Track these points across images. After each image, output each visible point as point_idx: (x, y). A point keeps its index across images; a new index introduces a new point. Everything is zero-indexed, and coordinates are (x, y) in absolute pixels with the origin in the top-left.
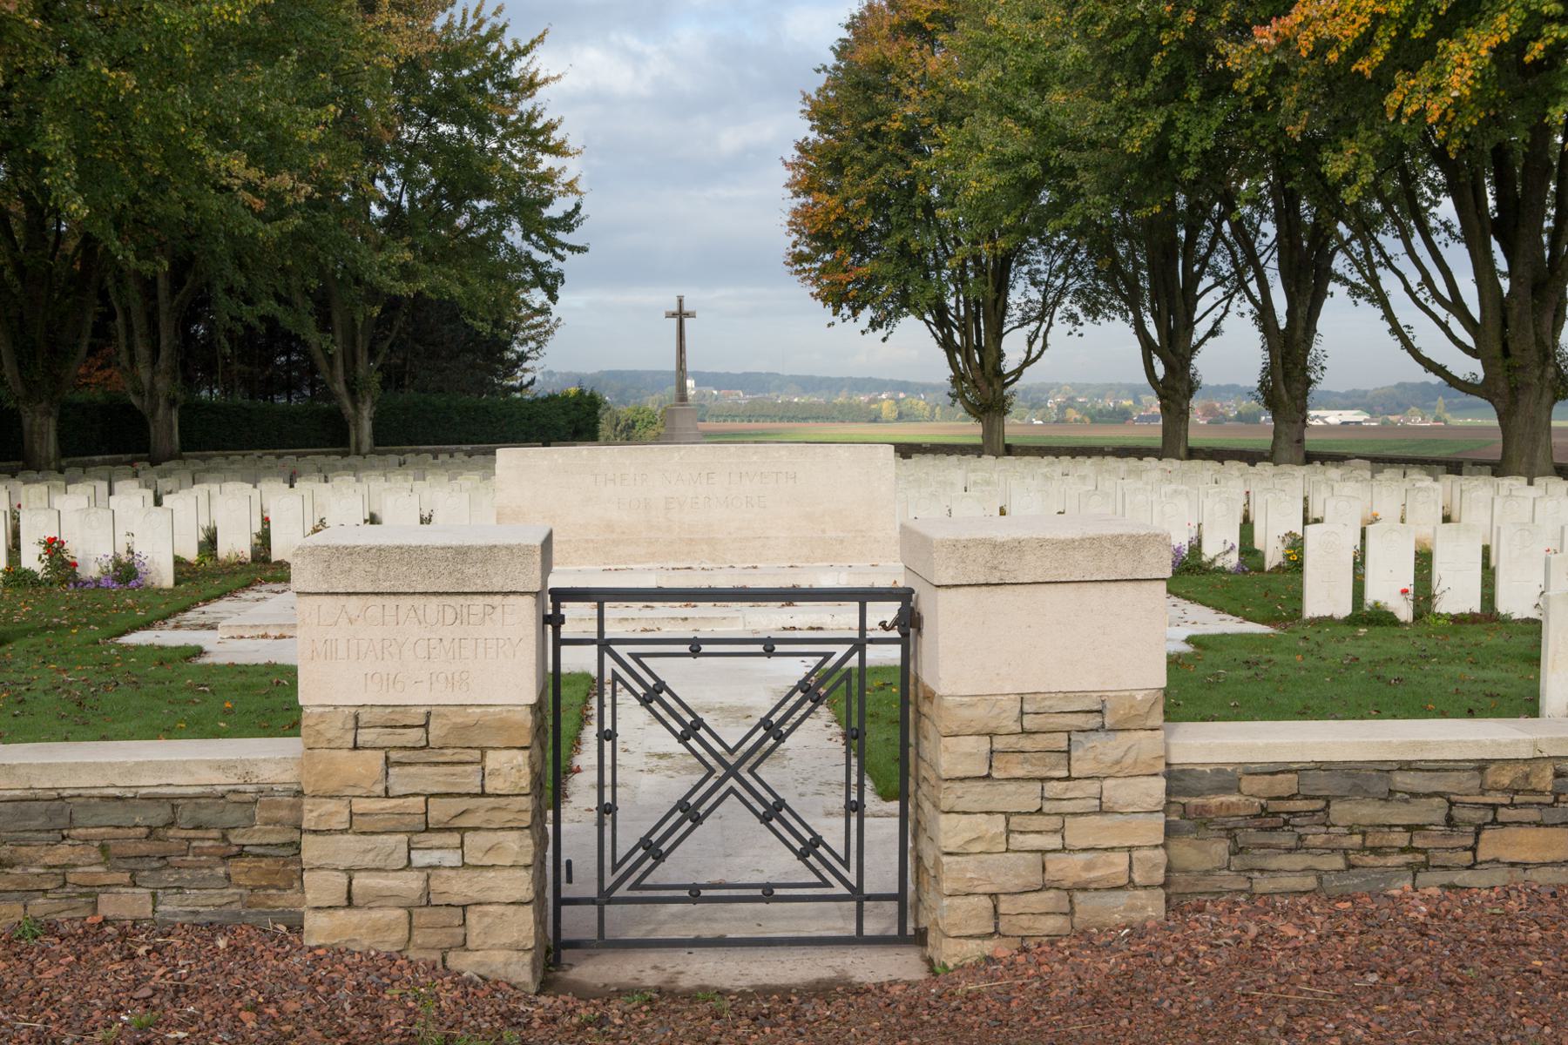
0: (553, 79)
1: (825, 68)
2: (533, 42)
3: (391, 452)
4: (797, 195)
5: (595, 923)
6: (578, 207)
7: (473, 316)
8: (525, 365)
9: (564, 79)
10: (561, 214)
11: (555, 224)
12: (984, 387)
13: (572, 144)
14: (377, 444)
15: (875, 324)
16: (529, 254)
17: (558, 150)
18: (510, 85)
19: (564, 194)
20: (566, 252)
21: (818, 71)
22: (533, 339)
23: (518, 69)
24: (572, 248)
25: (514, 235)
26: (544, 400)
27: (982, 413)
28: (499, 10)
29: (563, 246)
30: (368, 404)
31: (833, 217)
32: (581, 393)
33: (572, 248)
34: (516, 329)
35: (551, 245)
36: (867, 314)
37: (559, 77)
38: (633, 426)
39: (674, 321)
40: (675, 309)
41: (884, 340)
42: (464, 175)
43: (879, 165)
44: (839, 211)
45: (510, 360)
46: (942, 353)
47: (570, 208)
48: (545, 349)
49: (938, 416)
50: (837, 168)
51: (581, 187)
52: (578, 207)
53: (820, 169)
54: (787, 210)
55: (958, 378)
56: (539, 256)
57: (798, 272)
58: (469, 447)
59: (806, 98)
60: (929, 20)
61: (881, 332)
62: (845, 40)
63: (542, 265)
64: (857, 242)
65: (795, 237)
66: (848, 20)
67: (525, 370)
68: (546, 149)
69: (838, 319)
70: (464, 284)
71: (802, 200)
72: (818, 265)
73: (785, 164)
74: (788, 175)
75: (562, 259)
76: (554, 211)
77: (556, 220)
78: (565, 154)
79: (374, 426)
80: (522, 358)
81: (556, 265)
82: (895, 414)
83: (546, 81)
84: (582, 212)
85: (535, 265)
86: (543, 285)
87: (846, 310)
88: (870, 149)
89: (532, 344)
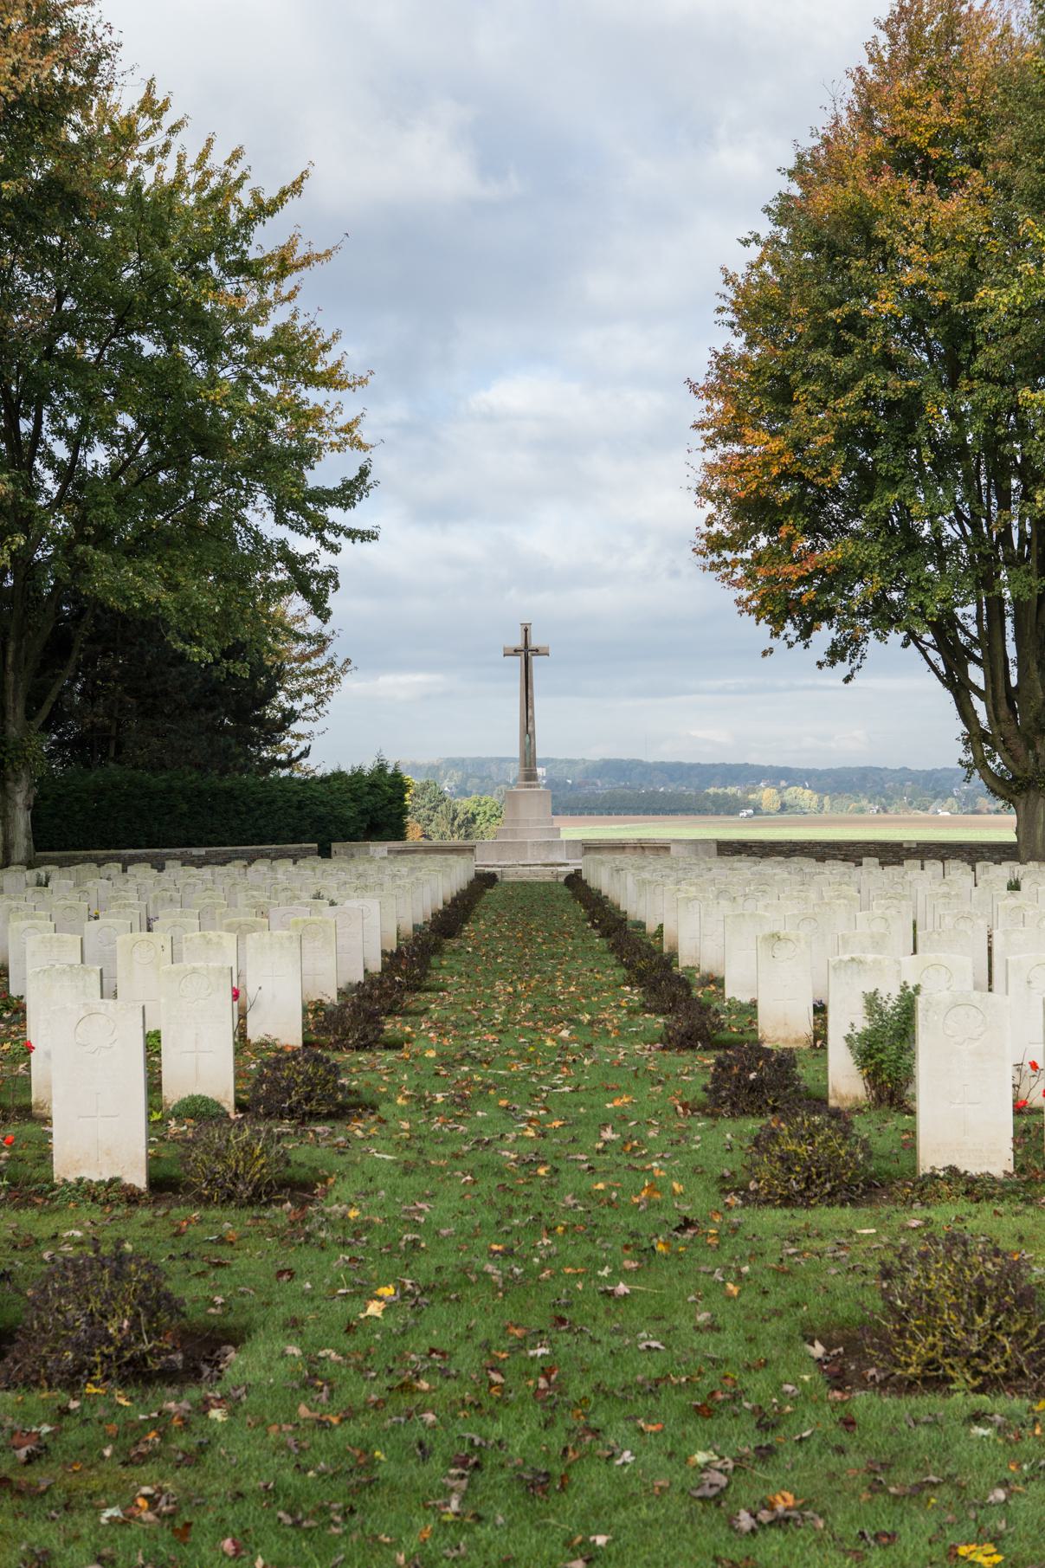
0: (319, 257)
1: (756, 239)
2: (284, 193)
3: (84, 860)
4: (710, 443)
5: (538, 702)
6: (364, 473)
7: (190, 638)
8: (296, 727)
9: (335, 256)
10: (338, 484)
11: (324, 497)
12: (1021, 751)
13: (352, 369)
14: (38, 848)
15: (836, 654)
16: (283, 545)
17: (329, 380)
18: (243, 268)
19: (338, 447)
20: (343, 541)
21: (746, 243)
22: (310, 691)
23: (263, 241)
24: (352, 534)
25: (260, 517)
26: (325, 780)
27: (1017, 792)
28: (236, 156)
29: (337, 529)
30: (24, 785)
31: (775, 471)
32: (381, 769)
33: (352, 534)
34: (280, 674)
35: (318, 527)
36: (825, 635)
37: (328, 253)
38: (473, 820)
39: (518, 661)
40: (518, 643)
41: (847, 679)
42: (184, 428)
43: (855, 378)
44: (786, 460)
45: (273, 721)
46: (948, 697)
47: (352, 474)
48: (328, 706)
49: (827, 807)
50: (783, 394)
51: (365, 434)
52: (364, 473)
53: (753, 394)
54: (698, 464)
55: (975, 737)
56: (302, 545)
57: (714, 567)
58: (202, 851)
59: (729, 280)
60: (933, 142)
61: (843, 668)
62: (789, 197)
63: (304, 560)
64: (812, 512)
65: (710, 508)
66: (791, 163)
67: (299, 737)
68: (313, 379)
69: (779, 644)
70: (173, 587)
71: (721, 449)
72: (748, 555)
73: (693, 388)
74: (697, 408)
75: (335, 549)
76: (324, 474)
77: (328, 492)
78: (340, 385)
79: (35, 820)
80: (291, 716)
81: (326, 560)
82: (777, 806)
83: (307, 261)
84: (369, 480)
85: (292, 561)
86: (306, 593)
87: (789, 628)
88: (842, 349)
89: (309, 699)
